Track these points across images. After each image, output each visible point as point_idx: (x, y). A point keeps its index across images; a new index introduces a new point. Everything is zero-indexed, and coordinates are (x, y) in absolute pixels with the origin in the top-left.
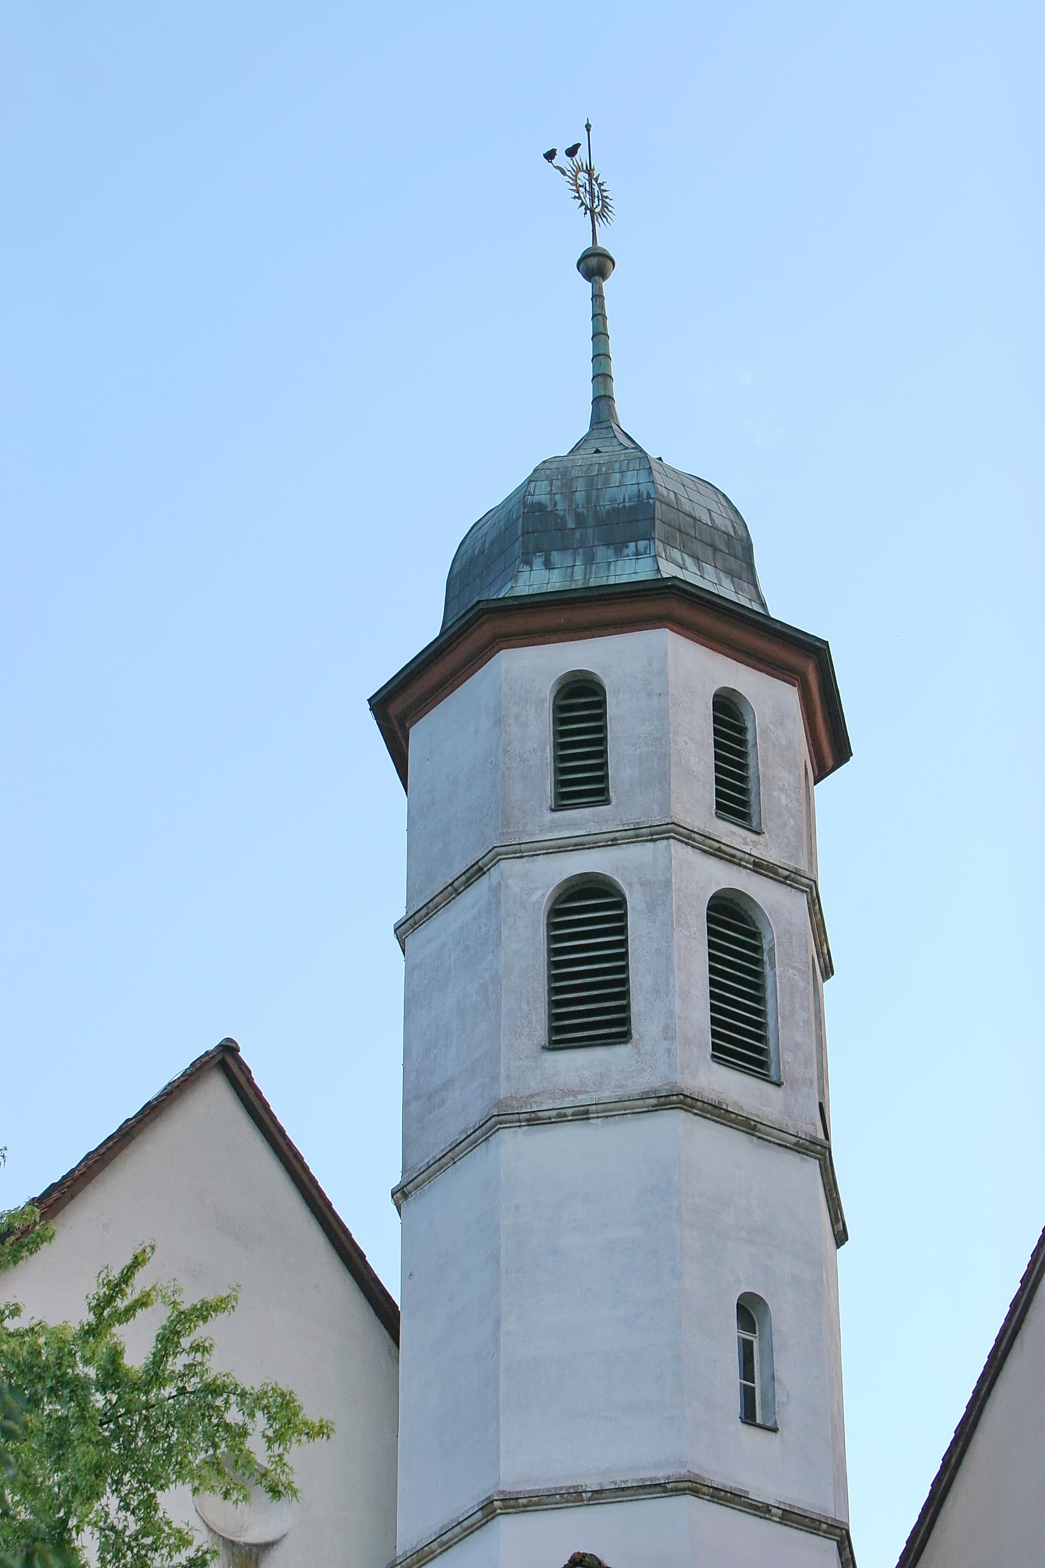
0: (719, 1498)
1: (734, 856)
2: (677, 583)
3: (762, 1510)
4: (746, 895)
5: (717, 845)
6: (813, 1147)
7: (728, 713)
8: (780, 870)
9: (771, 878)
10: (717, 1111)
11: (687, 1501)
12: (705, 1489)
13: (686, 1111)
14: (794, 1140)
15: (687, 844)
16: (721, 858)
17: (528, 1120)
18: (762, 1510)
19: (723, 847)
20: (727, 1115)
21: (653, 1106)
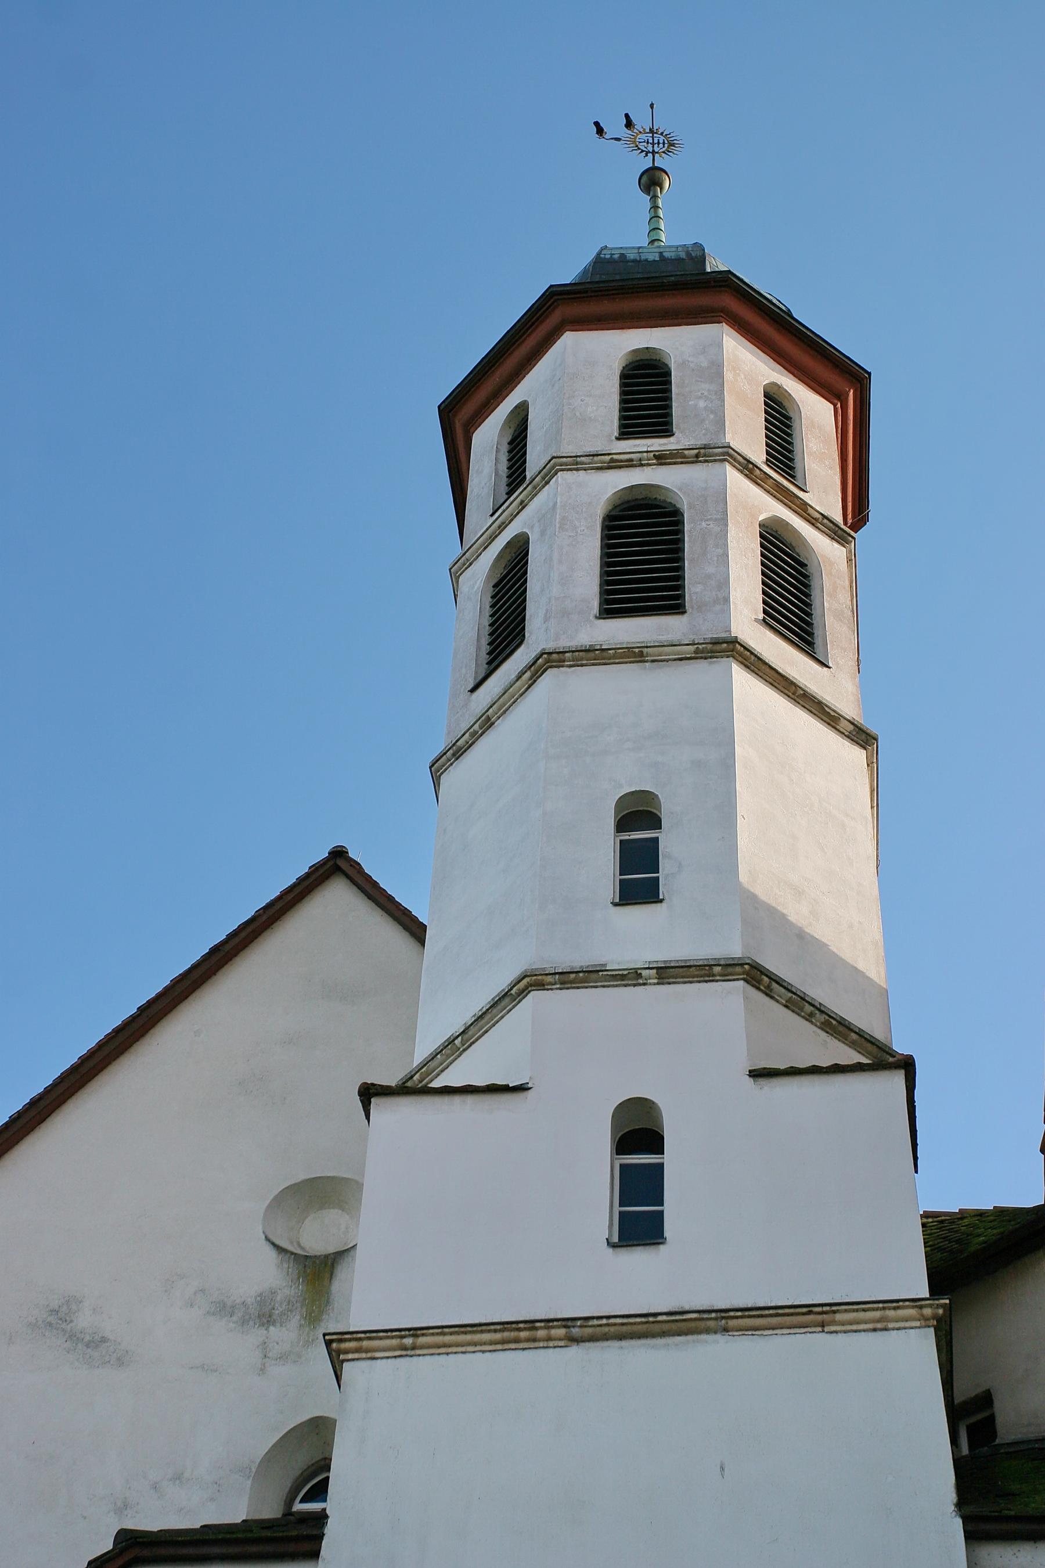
0: (571, 982)
1: (631, 460)
2: (555, 289)
3: (631, 977)
4: (652, 485)
5: (608, 458)
6: (718, 647)
7: (779, 418)
8: (686, 452)
9: (682, 463)
10: (592, 654)
11: (534, 997)
12: (549, 979)
13: (558, 667)
14: (692, 648)
15: (577, 470)
16: (620, 467)
17: (454, 755)
18: (631, 977)
19: (615, 457)
20: (605, 654)
21: (531, 678)
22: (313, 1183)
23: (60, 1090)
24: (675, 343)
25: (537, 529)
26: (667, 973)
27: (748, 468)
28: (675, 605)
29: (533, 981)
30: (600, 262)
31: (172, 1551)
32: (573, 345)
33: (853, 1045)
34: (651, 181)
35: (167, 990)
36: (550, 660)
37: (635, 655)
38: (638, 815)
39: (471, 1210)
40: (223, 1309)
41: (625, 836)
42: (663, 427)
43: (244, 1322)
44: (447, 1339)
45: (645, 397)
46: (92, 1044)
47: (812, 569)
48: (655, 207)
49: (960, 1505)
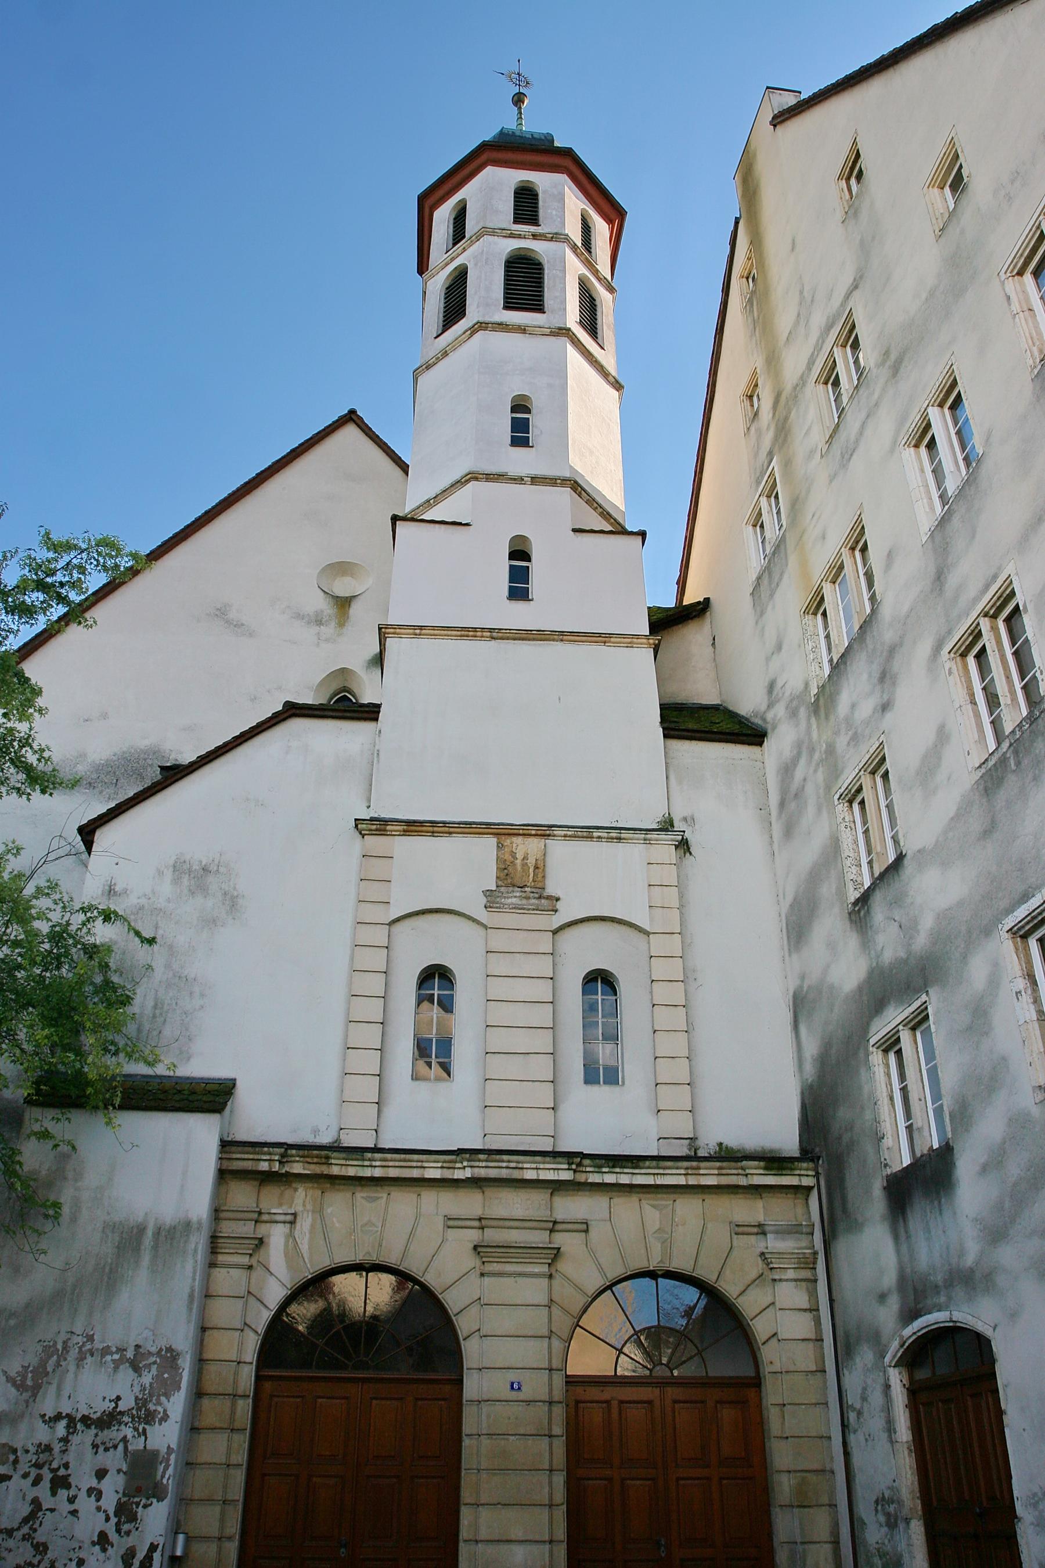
3: (519, 480)
18: (519, 480)
22: (341, 564)
23: (219, 508)
24: (543, 181)
25: (472, 262)
26: (535, 480)
27: (574, 248)
28: (539, 309)
29: (473, 477)
30: (502, 133)
31: (310, 712)
32: (490, 173)
33: (611, 524)
34: (518, 100)
35: (270, 467)
36: (481, 326)
37: (522, 330)
38: (520, 406)
39: (448, 575)
40: (299, 616)
41: (514, 415)
42: (534, 221)
43: (309, 623)
44: (436, 632)
45: (526, 205)
46: (234, 489)
47: (597, 303)
48: (520, 113)
49: (661, 723)
